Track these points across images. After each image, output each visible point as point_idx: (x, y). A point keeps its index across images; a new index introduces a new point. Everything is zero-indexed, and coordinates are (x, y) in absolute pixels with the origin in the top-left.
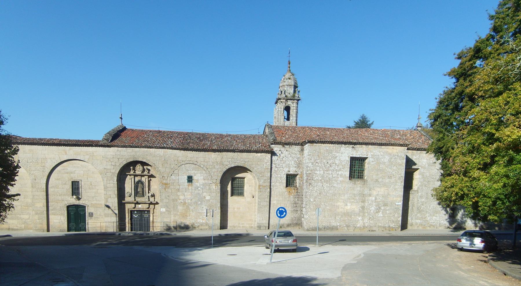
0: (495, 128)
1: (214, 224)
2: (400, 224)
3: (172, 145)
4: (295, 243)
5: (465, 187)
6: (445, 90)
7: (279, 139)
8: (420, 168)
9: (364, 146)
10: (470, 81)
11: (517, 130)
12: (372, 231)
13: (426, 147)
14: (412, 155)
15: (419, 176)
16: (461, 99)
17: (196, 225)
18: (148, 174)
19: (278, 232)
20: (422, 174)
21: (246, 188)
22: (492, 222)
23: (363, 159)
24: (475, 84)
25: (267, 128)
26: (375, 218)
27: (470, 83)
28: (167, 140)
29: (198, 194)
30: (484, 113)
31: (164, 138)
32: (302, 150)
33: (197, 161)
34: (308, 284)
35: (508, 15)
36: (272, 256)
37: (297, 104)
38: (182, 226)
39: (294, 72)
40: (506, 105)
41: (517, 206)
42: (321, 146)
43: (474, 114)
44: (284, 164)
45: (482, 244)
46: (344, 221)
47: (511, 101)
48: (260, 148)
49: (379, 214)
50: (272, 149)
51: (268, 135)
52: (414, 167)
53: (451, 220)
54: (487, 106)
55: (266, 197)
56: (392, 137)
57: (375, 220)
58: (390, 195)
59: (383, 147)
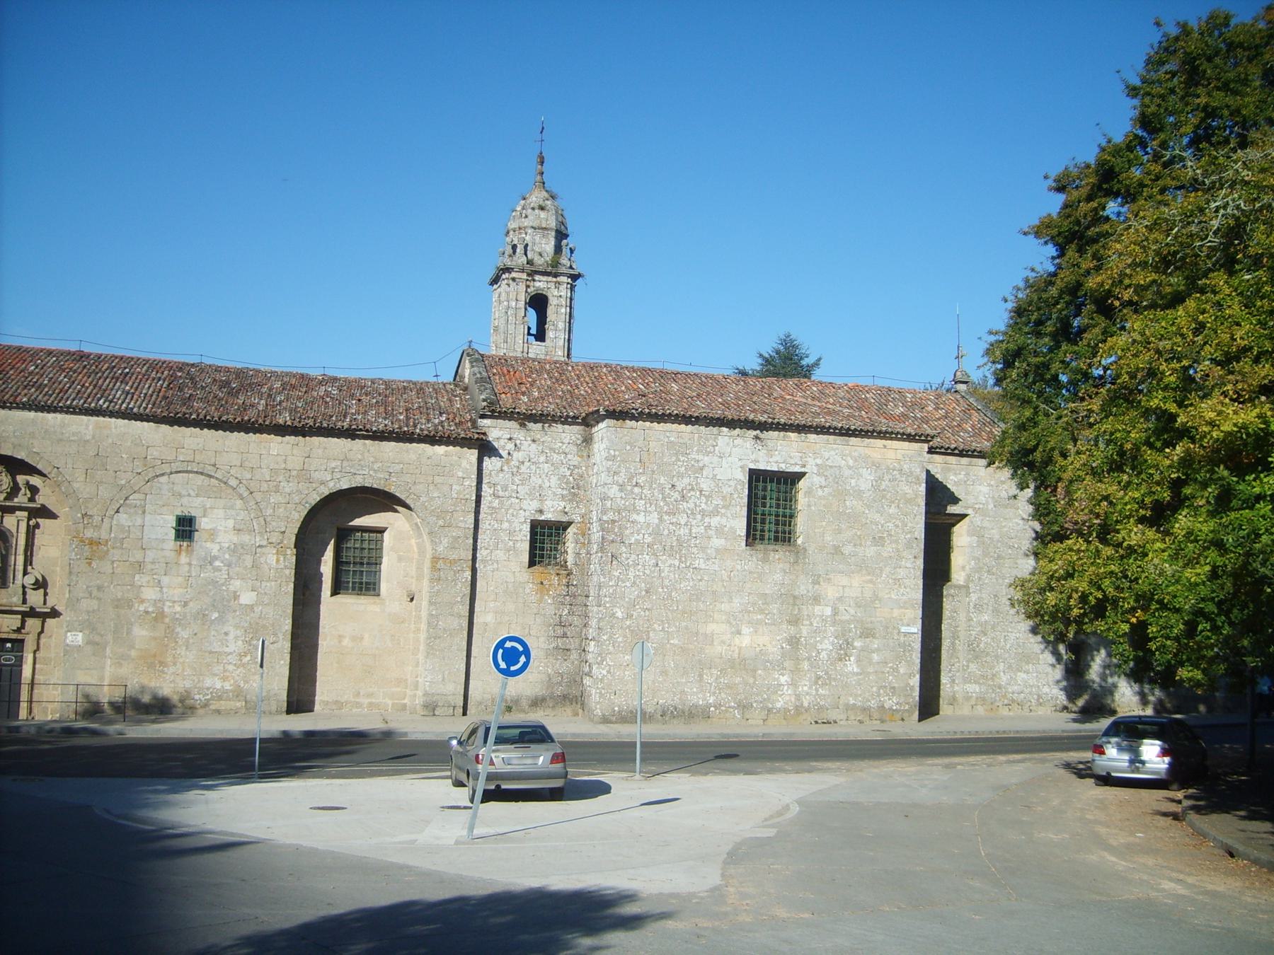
0: (1175, 397)
1: (264, 694)
2: (917, 698)
3: (129, 403)
4: (560, 765)
5: (1106, 578)
6: (1030, 278)
7: (506, 401)
8: (969, 511)
9: (793, 435)
10: (1096, 257)
11: (1234, 408)
12: (823, 723)
13: (986, 445)
14: (946, 470)
15: (969, 539)
16: (1076, 305)
17: (197, 697)
18: (30, 505)
19: (499, 728)
20: (977, 532)
21: (388, 564)
22: (1187, 689)
23: (791, 479)
24: (1111, 267)
25: (467, 361)
26: (835, 679)
27: (1095, 261)
28: (111, 386)
29: (214, 583)
30: (1141, 352)
31: (100, 378)
32: (588, 440)
33: (214, 465)
34: (606, 917)
35: (1172, 91)
36: (474, 816)
37: (572, 288)
38: (143, 700)
39: (555, 190)
40: (1197, 332)
41: (1251, 638)
42: (650, 429)
43: (1116, 353)
44: (522, 484)
45: (1164, 761)
46: (731, 688)
47: (1208, 322)
48: (443, 427)
49: (848, 663)
50: (484, 434)
51: (470, 387)
52: (952, 509)
53: (1072, 683)
54: (1147, 332)
55: (459, 599)
56: (881, 411)
57: (834, 683)
58: (880, 600)
59: (853, 440)
